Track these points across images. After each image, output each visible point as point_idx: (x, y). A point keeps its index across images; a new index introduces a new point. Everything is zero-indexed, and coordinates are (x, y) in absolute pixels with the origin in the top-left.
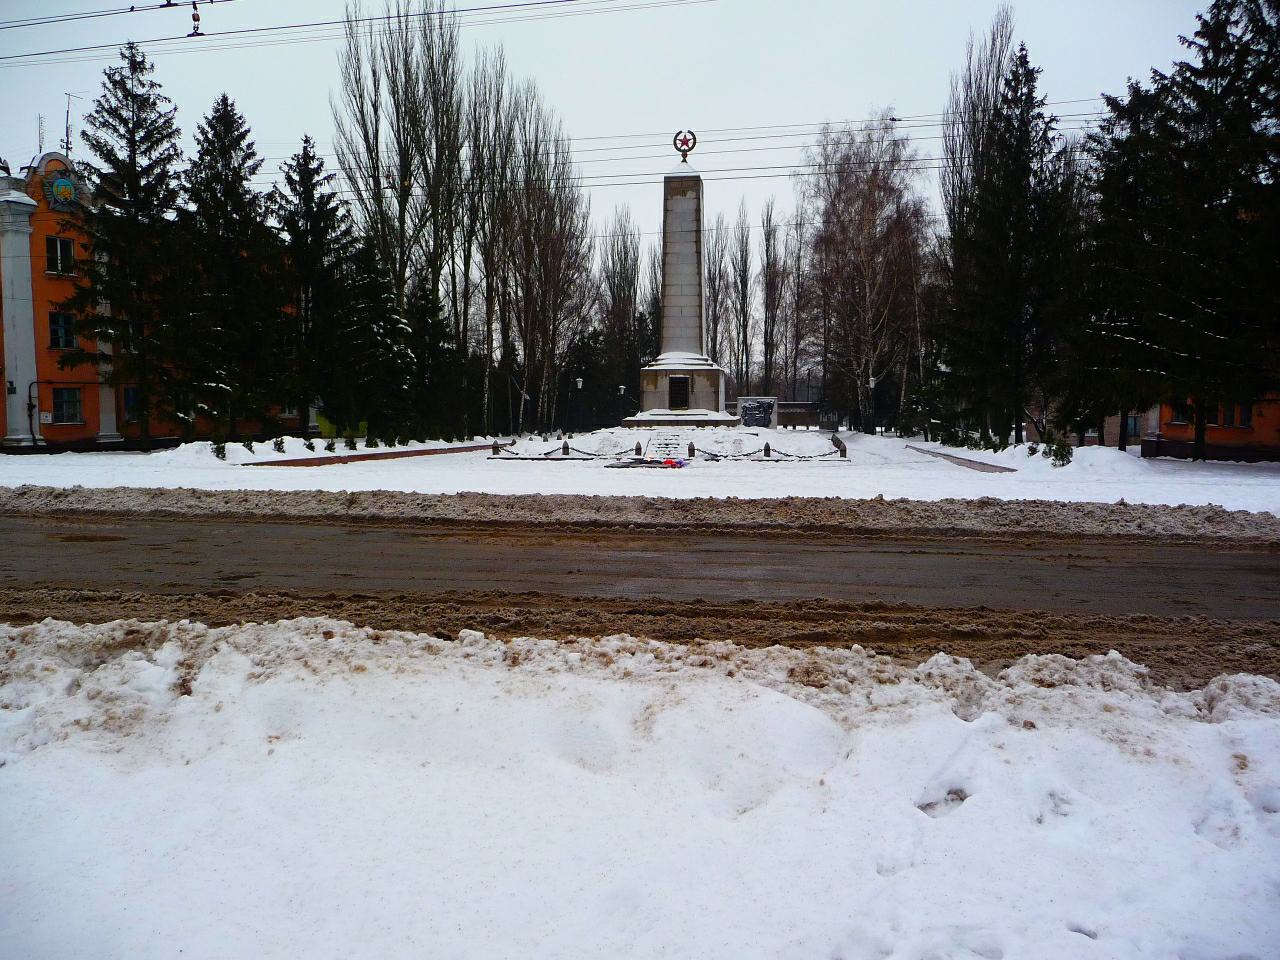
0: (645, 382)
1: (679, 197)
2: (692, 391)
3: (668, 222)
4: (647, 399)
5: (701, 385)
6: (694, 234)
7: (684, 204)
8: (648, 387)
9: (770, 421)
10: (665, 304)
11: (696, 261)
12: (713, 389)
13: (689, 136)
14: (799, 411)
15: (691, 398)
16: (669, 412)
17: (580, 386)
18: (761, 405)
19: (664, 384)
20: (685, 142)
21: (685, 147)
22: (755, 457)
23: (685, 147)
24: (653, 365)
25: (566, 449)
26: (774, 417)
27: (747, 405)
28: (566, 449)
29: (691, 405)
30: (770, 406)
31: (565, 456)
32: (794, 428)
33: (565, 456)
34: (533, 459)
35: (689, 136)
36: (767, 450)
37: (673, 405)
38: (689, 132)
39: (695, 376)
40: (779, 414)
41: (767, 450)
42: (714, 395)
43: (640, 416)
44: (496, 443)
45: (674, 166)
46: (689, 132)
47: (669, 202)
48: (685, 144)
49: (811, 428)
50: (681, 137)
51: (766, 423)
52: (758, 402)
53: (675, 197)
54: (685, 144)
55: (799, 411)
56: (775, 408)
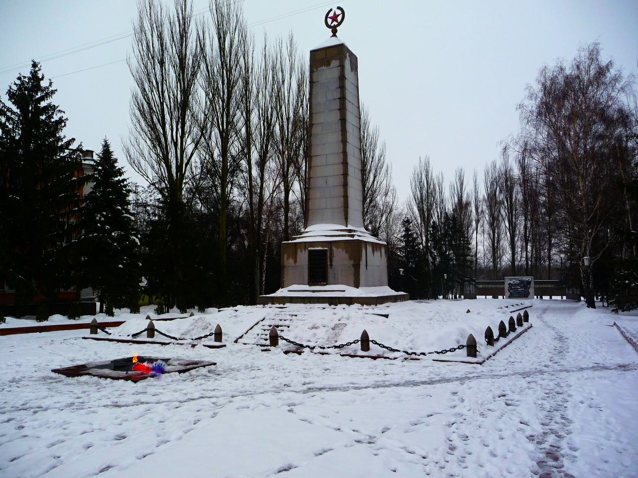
0: (286, 256)
1: (324, 68)
2: (331, 265)
3: (314, 93)
4: (288, 274)
5: (340, 258)
6: (338, 102)
7: (329, 74)
8: (288, 262)
9: (529, 294)
10: (311, 176)
11: (340, 128)
12: (352, 262)
13: (338, 12)
14: (550, 286)
15: (330, 272)
16: (307, 287)
17: (446, 278)
18: (522, 282)
19: (303, 257)
20: (334, 18)
21: (335, 23)
22: (350, 350)
23: (335, 23)
24: (295, 239)
25: (151, 331)
26: (531, 291)
27: (512, 282)
28: (151, 331)
29: (330, 279)
30: (529, 283)
31: (150, 340)
32: (551, 298)
33: (150, 340)
34: (118, 341)
35: (338, 12)
36: (365, 341)
37: (311, 283)
38: (339, 8)
39: (334, 248)
40: (535, 289)
41: (365, 341)
42: (352, 270)
43: (281, 293)
44: (95, 320)
45: (324, 39)
46: (339, 8)
47: (315, 74)
48: (334, 21)
49: (554, 298)
50: (331, 14)
51: (525, 295)
52: (520, 280)
53: (319, 69)
54: (334, 21)
55: (550, 286)
56: (532, 284)
